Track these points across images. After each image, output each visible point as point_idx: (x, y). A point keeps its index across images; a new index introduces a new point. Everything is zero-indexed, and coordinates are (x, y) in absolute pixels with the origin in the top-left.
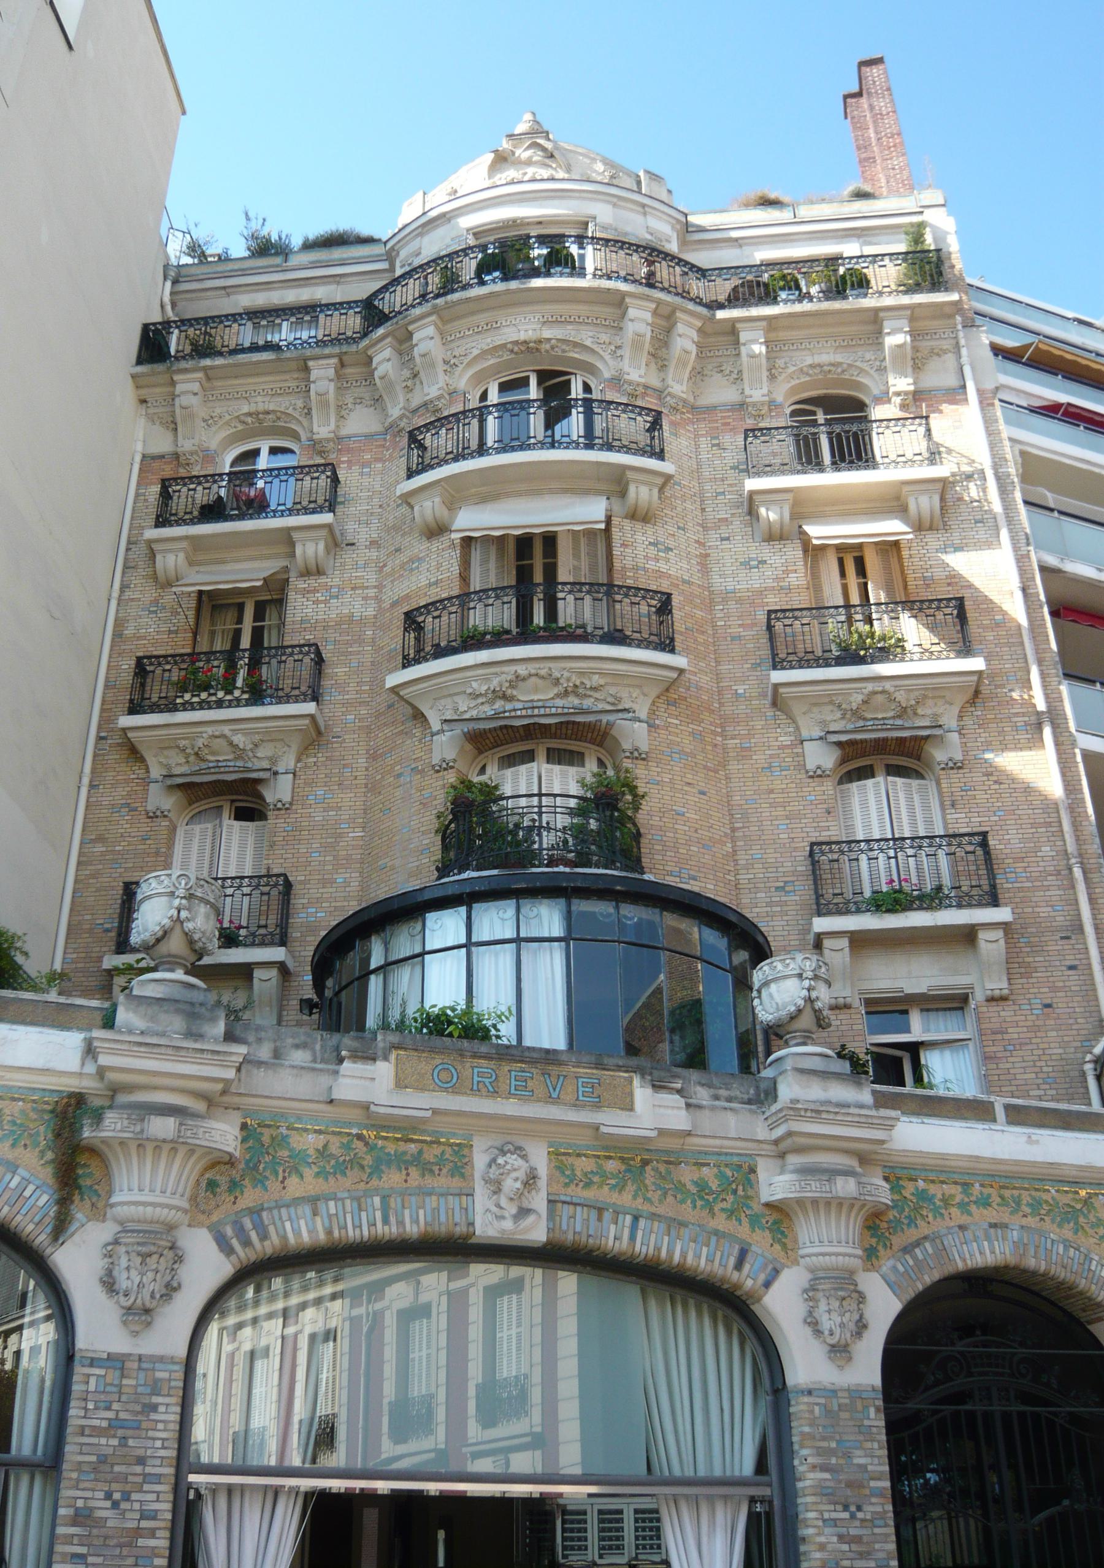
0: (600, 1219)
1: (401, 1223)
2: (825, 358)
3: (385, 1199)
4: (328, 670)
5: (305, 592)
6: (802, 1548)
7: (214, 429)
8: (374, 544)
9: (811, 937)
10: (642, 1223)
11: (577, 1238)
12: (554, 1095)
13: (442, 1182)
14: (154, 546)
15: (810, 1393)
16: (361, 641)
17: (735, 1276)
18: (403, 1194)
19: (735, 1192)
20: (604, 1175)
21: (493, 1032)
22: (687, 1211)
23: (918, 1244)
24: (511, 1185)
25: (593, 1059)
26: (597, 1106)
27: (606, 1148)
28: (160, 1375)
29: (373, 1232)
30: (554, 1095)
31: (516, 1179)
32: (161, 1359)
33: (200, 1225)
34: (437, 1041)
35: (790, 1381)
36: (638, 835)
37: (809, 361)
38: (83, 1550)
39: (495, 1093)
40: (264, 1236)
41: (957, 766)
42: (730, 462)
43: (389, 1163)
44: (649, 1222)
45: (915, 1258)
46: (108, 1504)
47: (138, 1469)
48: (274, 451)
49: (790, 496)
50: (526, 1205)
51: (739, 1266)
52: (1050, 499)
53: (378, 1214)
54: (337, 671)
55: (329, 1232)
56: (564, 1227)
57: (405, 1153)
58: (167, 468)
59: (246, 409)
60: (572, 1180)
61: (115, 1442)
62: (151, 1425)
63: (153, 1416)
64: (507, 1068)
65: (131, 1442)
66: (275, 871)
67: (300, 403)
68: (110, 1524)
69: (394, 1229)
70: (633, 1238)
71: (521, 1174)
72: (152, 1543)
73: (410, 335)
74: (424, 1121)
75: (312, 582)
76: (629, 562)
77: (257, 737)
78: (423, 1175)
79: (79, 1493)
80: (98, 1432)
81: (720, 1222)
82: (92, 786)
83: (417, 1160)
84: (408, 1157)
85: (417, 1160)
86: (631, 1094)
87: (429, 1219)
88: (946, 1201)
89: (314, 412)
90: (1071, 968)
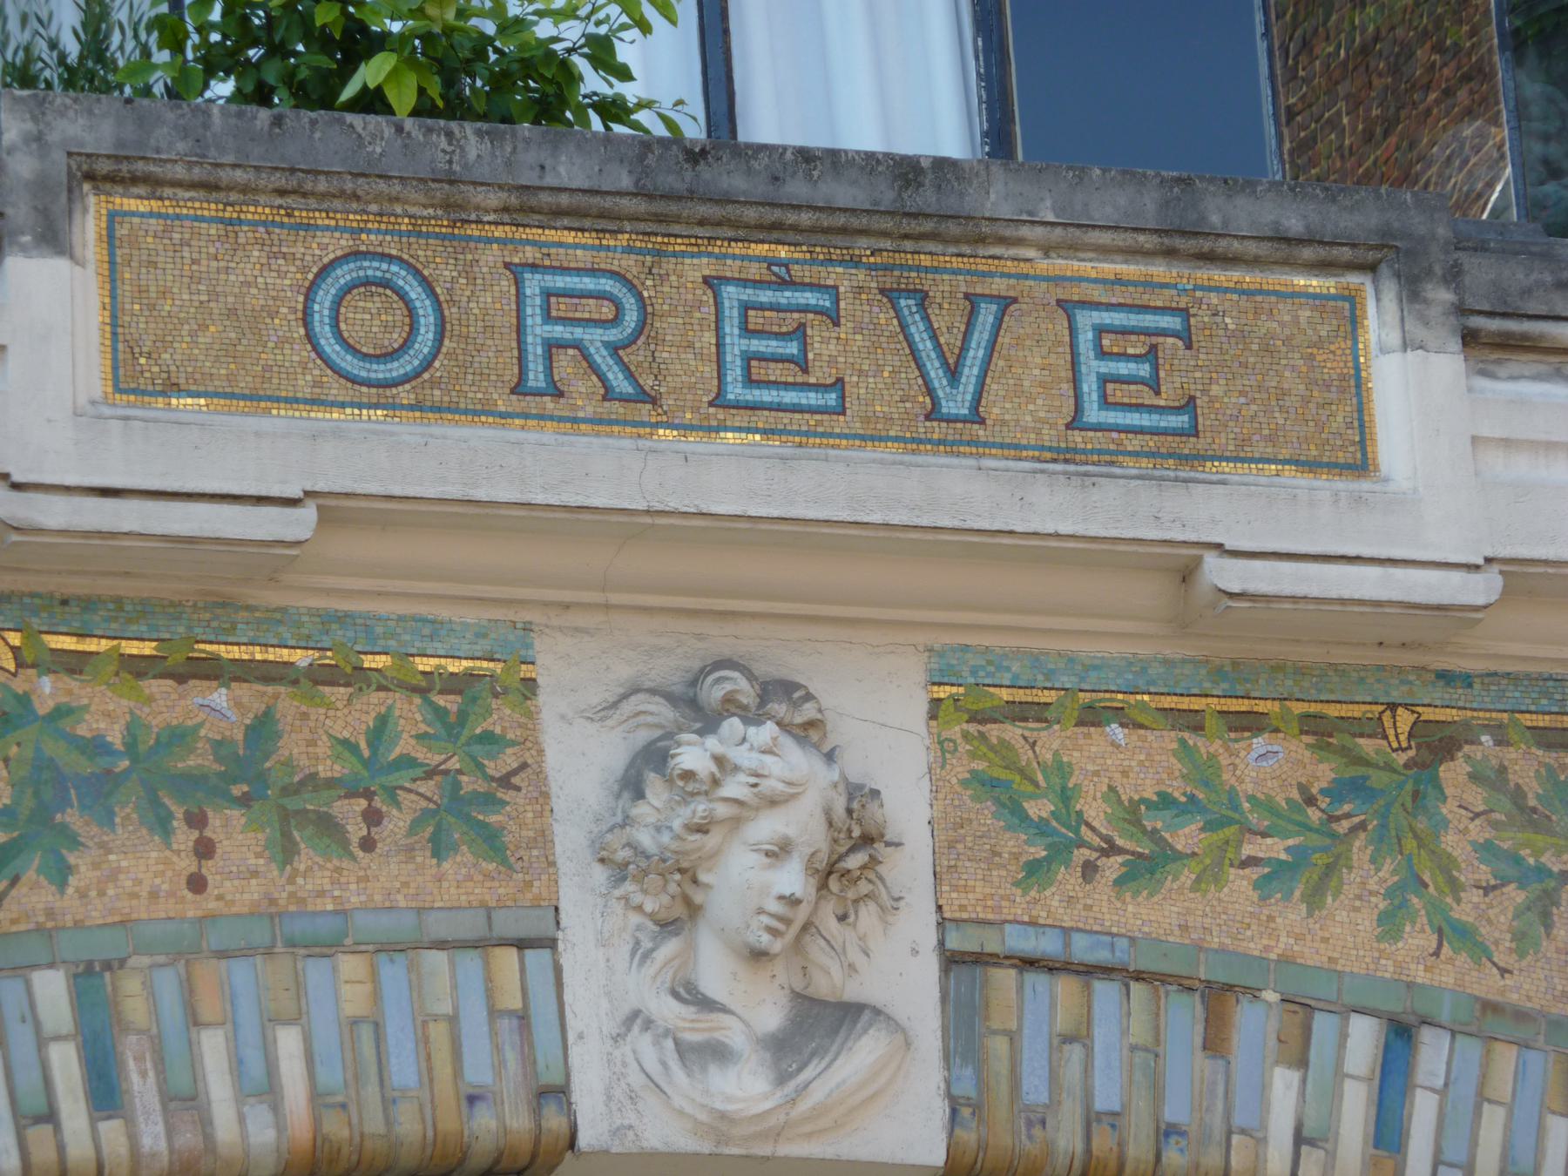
0: (1215, 1041)
1: (185, 1101)
3: (90, 979)
10: (1433, 1054)
11: (1103, 1142)
12: (956, 403)
13: (389, 879)
18: (186, 951)
20: (1224, 815)
21: (593, 82)
24: (752, 879)
25: (1149, 205)
26: (1184, 447)
27: (1232, 673)
29: (188, 1139)
30: (956, 403)
31: (779, 851)
34: (320, 137)
39: (639, 403)
43: (100, 792)
44: (1471, 1049)
50: (831, 982)
53: (65, 1062)
56: (1035, 1089)
57: (179, 737)
60: (1059, 846)
64: (697, 268)
69: (153, 1137)
71: (802, 823)
74: (272, 559)
78: (286, 852)
83: (246, 772)
84: (198, 760)
85: (246, 772)
86: (1356, 385)
87: (331, 1076)
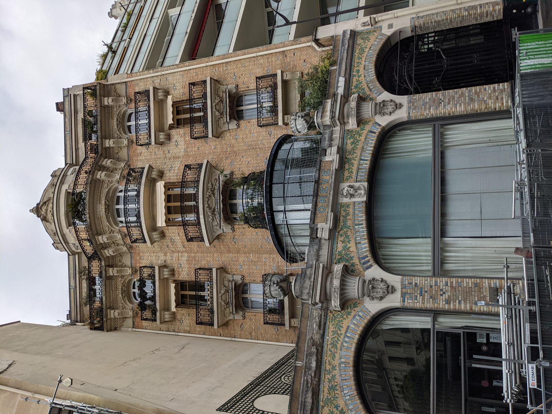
1: (362, 220)
2: (115, 123)
3: (356, 225)
4: (203, 266)
5: (179, 275)
6: (452, 115)
7: (126, 306)
8: (165, 255)
9: (284, 126)
13: (351, 210)
14: (162, 321)
15: (409, 113)
16: (195, 257)
17: (377, 134)
19: (354, 135)
22: (360, 146)
23: (369, 88)
28: (406, 283)
32: (402, 283)
33: (364, 274)
35: (406, 119)
36: (254, 173)
37: (116, 127)
38: (457, 301)
40: (367, 256)
41: (237, 86)
42: (146, 150)
45: (373, 88)
46: (444, 295)
47: (434, 287)
48: (134, 288)
49: (157, 133)
51: (375, 133)
52: (160, 60)
53: (360, 226)
54: (203, 264)
55: (365, 239)
58: (137, 320)
59: (121, 296)
60: (350, 177)
61: (426, 294)
62: (421, 285)
63: (418, 284)
65: (426, 290)
66: (262, 279)
67: (120, 279)
68: (449, 294)
70: (367, 160)
71: (349, 189)
72: (454, 282)
73: (101, 244)
75: (176, 273)
76: (175, 178)
77: (222, 286)
79: (441, 303)
80: (423, 299)
81: (362, 138)
82: (235, 337)
88: (357, 81)
89: (123, 274)
90: (294, 55)
